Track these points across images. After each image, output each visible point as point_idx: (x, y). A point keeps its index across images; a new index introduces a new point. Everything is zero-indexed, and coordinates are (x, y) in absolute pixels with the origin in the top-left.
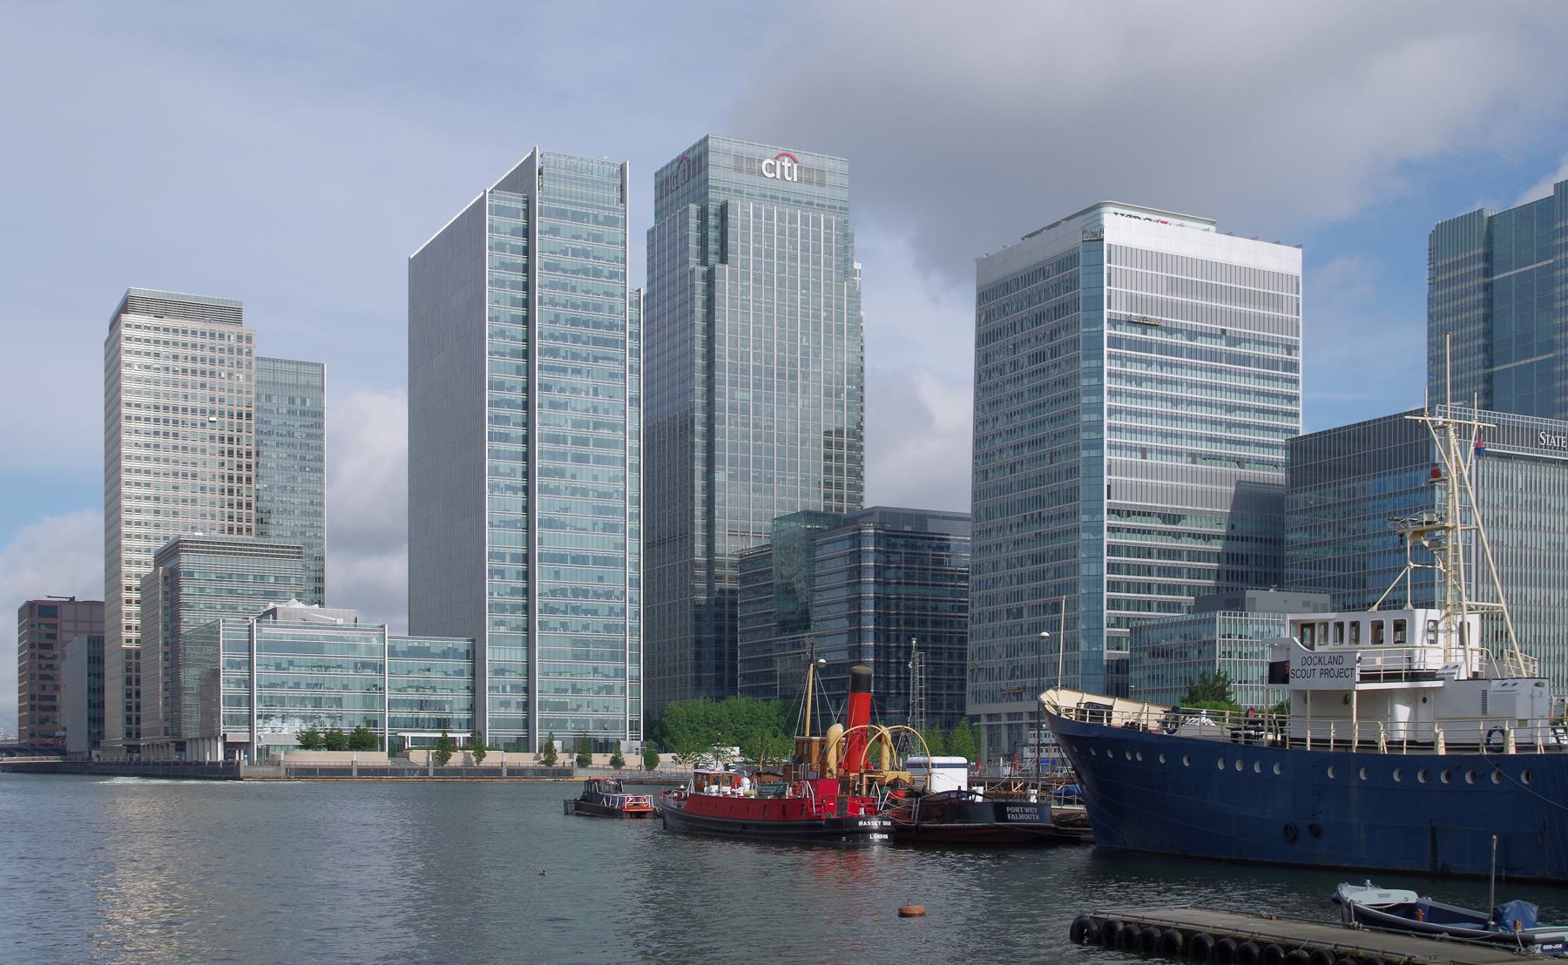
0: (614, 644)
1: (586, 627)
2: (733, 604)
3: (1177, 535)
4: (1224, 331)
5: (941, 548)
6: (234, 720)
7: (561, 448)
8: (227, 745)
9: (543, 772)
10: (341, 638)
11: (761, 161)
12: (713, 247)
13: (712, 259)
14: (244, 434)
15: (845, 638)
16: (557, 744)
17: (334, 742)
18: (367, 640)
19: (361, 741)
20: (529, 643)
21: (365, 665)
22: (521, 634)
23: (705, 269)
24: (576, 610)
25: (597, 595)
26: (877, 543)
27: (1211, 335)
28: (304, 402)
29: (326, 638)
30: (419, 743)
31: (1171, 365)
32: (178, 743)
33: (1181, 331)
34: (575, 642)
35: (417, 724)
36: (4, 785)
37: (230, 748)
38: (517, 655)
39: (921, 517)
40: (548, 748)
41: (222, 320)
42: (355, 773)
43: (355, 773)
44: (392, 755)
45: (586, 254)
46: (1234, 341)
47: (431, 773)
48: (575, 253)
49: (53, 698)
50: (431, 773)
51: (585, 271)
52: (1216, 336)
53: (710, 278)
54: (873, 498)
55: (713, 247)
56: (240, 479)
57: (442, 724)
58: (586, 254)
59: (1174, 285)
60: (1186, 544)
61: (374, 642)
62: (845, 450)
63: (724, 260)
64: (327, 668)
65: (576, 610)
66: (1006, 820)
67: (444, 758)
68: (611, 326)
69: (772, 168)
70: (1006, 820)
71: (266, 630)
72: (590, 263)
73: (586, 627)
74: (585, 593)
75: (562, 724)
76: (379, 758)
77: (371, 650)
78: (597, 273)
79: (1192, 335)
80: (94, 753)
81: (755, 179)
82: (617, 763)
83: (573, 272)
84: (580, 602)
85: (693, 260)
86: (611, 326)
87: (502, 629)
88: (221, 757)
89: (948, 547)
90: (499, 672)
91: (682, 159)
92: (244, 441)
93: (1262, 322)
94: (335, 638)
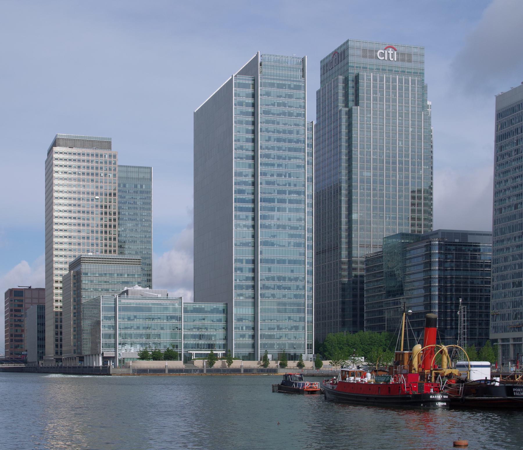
0: (299, 304)
1: (284, 296)
2: (362, 282)
5: (475, 251)
6: (108, 346)
7: (272, 205)
8: (104, 358)
9: (262, 371)
10: (160, 304)
11: (377, 51)
12: (351, 97)
13: (351, 104)
14: (112, 204)
15: (422, 299)
16: (269, 356)
17: (156, 357)
18: (173, 305)
19: (170, 356)
20: (255, 305)
21: (172, 318)
22: (251, 300)
23: (347, 109)
25: (290, 279)
26: (440, 249)
30: (199, 356)
32: (80, 357)
34: (279, 304)
35: (198, 346)
37: (106, 359)
38: (249, 311)
39: (464, 235)
40: (265, 358)
42: (167, 372)
43: (167, 372)
44: (185, 362)
45: (284, 105)
47: (205, 371)
48: (279, 105)
49: (21, 336)
50: (205, 371)
51: (284, 114)
53: (350, 114)
54: (436, 226)
55: (351, 97)
57: (211, 346)
58: (284, 105)
61: (177, 306)
62: (422, 199)
63: (357, 104)
66: (513, 395)
67: (211, 364)
68: (298, 141)
69: (383, 55)
70: (513, 395)
71: (123, 301)
72: (287, 109)
74: (284, 279)
75: (272, 346)
76: (179, 364)
77: (175, 310)
78: (290, 114)
80: (40, 362)
81: (374, 61)
82: (300, 366)
83: (278, 115)
84: (281, 283)
85: (341, 105)
86: (298, 141)
87: (241, 298)
88: (101, 364)
89: (480, 250)
90: (240, 320)
91: (335, 53)
94: (158, 304)
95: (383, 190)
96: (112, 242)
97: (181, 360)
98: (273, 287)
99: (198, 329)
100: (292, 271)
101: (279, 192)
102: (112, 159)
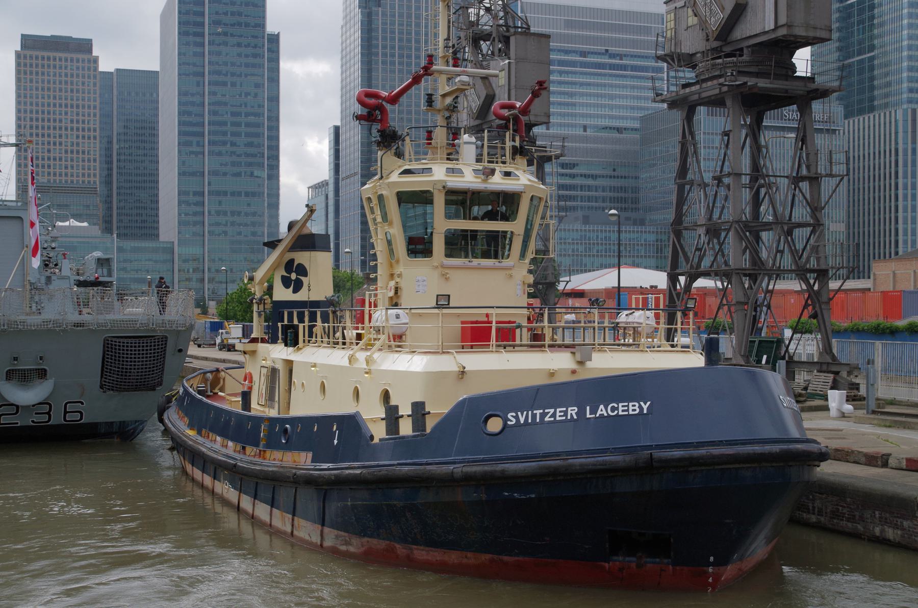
1: (240, 233)
3: (573, 176)
4: (607, 51)
7: (224, 128)
10: (88, 243)
14: (92, 118)
24: (233, 224)
25: (247, 214)
27: (599, 54)
28: (144, 95)
29: (78, 242)
31: (567, 73)
33: (574, 52)
36: (915, 494)
41: (57, 50)
45: (240, 14)
46: (613, 56)
48: (233, 14)
51: (240, 24)
52: (603, 54)
56: (72, 152)
58: (240, 14)
59: (569, 24)
60: (578, 181)
64: (131, 262)
65: (233, 224)
72: (243, 19)
73: (240, 233)
74: (239, 213)
78: (247, 25)
79: (583, 54)
83: (231, 25)
84: (236, 219)
92: (92, 122)
93: (635, 44)
95: (411, 106)
96: (92, 163)
97: (869, 278)
98: (224, 222)
99: (137, 271)
100: (249, 205)
101: (234, 114)
102: (92, 65)
